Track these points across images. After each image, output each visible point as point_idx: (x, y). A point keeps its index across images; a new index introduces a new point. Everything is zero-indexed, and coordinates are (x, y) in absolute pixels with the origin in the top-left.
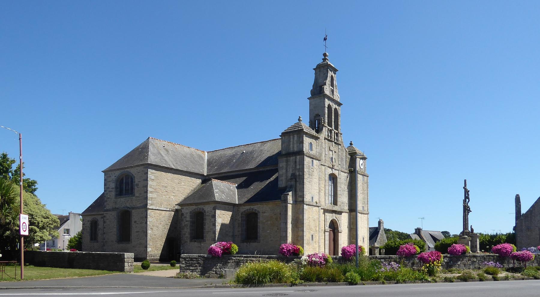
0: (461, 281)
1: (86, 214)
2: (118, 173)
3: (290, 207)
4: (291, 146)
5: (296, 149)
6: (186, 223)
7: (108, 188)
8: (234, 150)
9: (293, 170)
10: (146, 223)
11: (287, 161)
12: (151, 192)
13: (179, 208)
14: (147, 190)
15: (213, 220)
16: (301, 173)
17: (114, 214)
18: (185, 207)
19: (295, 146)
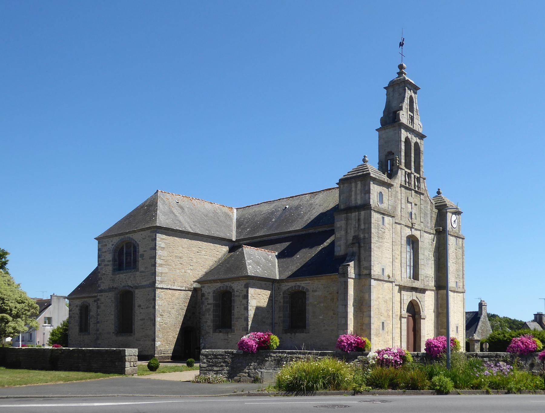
2: (116, 240)
3: (351, 283)
4: (353, 197)
5: (359, 202)
7: (104, 261)
8: (273, 205)
9: (355, 231)
11: (347, 219)
12: (161, 265)
14: (155, 263)
15: (244, 301)
16: (366, 235)
17: (111, 295)
18: (206, 285)
19: (359, 197)
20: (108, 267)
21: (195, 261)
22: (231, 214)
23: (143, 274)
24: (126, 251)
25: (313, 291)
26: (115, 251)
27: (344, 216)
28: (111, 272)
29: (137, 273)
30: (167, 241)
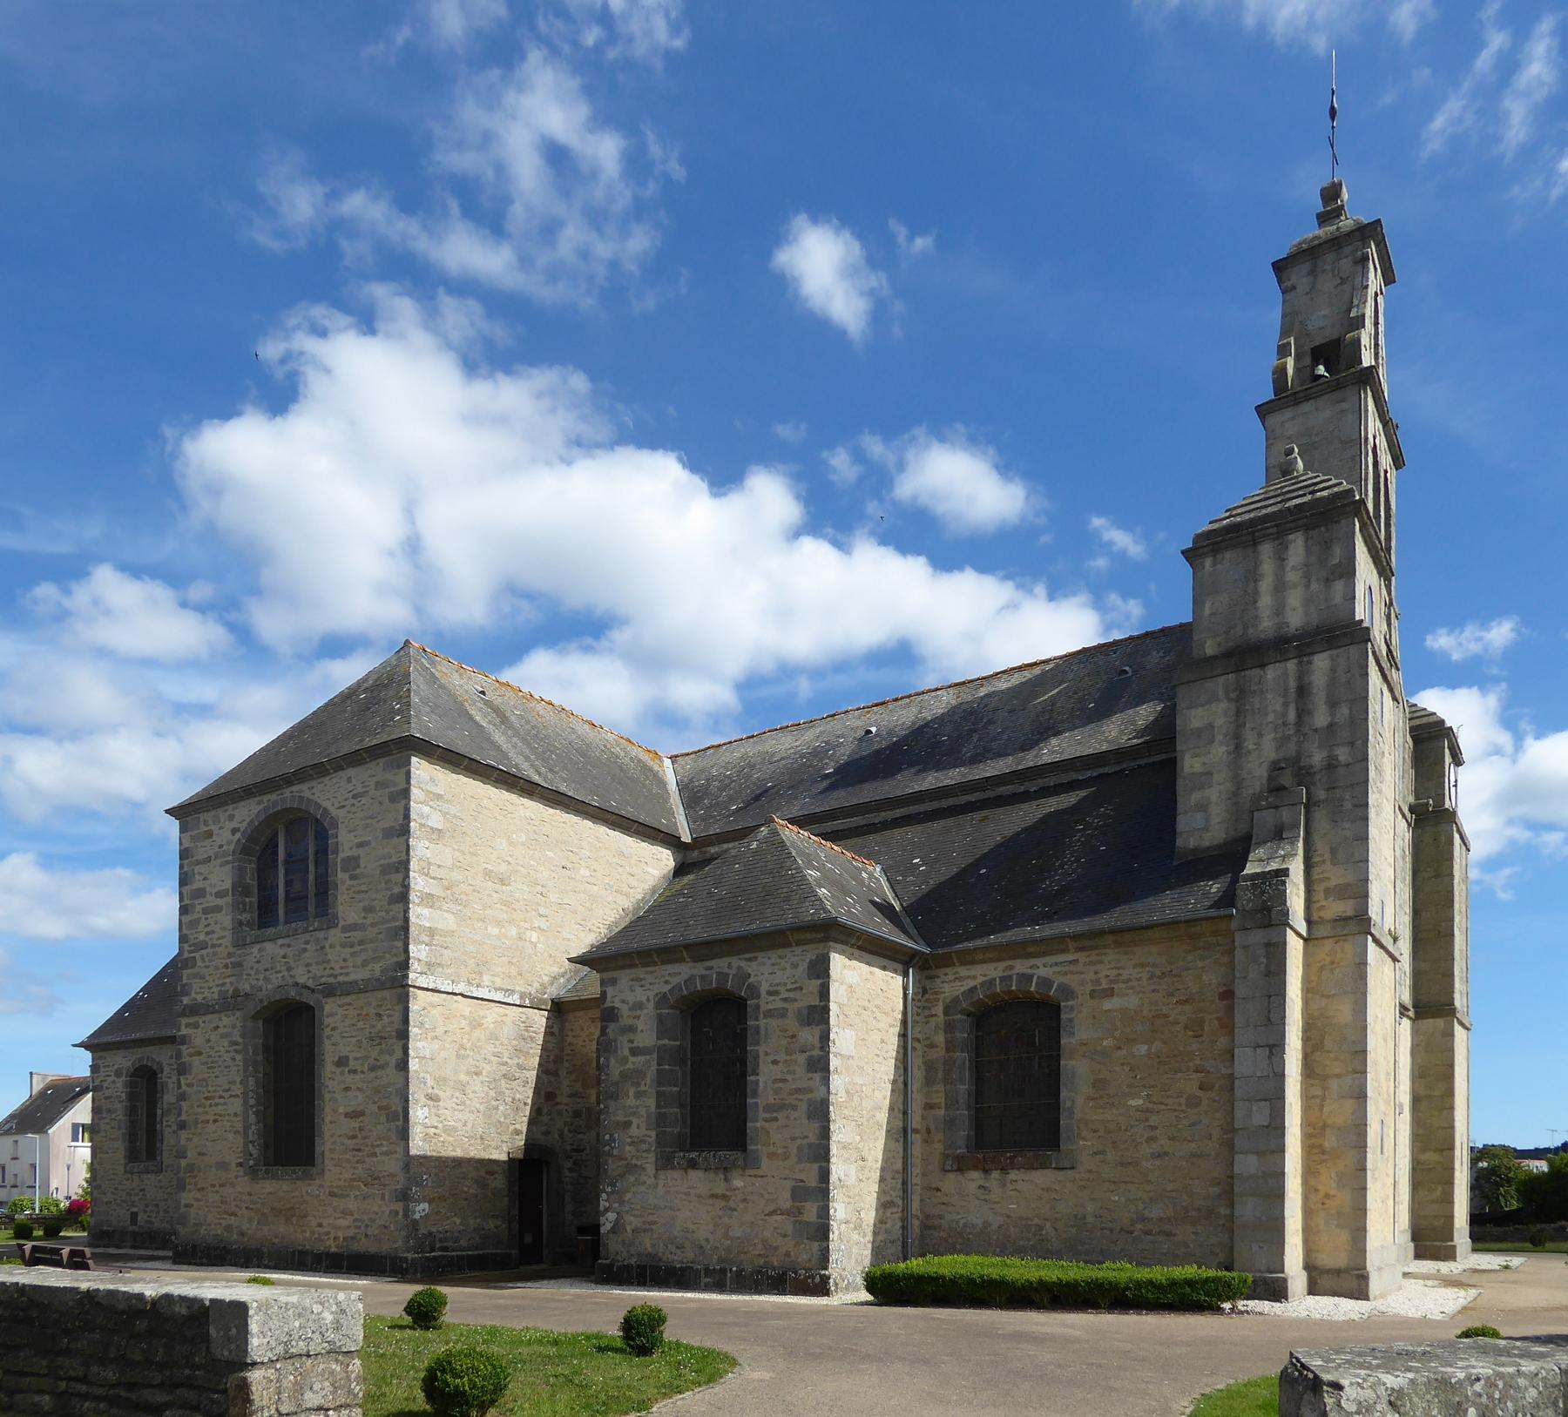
0: (1439, 1286)
1: (108, 1039)
2: (246, 813)
3: (1295, 948)
4: (1266, 601)
5: (1295, 619)
6: (635, 1062)
7: (200, 893)
8: (809, 735)
9: (1281, 742)
10: (403, 1066)
11: (1241, 695)
12: (429, 900)
13: (592, 984)
14: (406, 888)
15: (809, 1035)
16: (1343, 754)
17: (230, 1022)
18: (624, 977)
19: (1294, 599)
20: (219, 916)
21: (553, 897)
22: (656, 768)
23: (356, 935)
24: (288, 854)
25: (1093, 994)
26: (245, 850)
27: (1220, 684)
28: (228, 933)
29: (333, 932)
30: (453, 810)
